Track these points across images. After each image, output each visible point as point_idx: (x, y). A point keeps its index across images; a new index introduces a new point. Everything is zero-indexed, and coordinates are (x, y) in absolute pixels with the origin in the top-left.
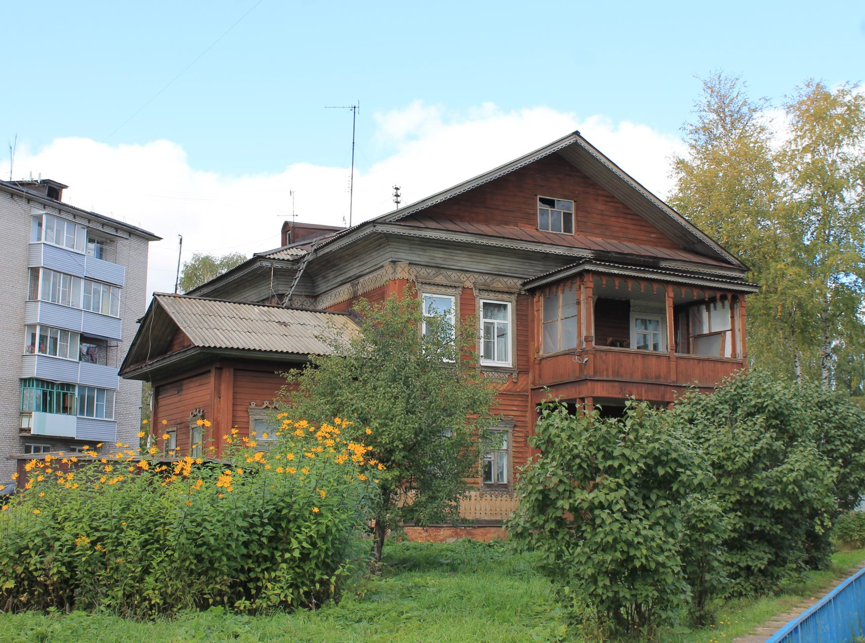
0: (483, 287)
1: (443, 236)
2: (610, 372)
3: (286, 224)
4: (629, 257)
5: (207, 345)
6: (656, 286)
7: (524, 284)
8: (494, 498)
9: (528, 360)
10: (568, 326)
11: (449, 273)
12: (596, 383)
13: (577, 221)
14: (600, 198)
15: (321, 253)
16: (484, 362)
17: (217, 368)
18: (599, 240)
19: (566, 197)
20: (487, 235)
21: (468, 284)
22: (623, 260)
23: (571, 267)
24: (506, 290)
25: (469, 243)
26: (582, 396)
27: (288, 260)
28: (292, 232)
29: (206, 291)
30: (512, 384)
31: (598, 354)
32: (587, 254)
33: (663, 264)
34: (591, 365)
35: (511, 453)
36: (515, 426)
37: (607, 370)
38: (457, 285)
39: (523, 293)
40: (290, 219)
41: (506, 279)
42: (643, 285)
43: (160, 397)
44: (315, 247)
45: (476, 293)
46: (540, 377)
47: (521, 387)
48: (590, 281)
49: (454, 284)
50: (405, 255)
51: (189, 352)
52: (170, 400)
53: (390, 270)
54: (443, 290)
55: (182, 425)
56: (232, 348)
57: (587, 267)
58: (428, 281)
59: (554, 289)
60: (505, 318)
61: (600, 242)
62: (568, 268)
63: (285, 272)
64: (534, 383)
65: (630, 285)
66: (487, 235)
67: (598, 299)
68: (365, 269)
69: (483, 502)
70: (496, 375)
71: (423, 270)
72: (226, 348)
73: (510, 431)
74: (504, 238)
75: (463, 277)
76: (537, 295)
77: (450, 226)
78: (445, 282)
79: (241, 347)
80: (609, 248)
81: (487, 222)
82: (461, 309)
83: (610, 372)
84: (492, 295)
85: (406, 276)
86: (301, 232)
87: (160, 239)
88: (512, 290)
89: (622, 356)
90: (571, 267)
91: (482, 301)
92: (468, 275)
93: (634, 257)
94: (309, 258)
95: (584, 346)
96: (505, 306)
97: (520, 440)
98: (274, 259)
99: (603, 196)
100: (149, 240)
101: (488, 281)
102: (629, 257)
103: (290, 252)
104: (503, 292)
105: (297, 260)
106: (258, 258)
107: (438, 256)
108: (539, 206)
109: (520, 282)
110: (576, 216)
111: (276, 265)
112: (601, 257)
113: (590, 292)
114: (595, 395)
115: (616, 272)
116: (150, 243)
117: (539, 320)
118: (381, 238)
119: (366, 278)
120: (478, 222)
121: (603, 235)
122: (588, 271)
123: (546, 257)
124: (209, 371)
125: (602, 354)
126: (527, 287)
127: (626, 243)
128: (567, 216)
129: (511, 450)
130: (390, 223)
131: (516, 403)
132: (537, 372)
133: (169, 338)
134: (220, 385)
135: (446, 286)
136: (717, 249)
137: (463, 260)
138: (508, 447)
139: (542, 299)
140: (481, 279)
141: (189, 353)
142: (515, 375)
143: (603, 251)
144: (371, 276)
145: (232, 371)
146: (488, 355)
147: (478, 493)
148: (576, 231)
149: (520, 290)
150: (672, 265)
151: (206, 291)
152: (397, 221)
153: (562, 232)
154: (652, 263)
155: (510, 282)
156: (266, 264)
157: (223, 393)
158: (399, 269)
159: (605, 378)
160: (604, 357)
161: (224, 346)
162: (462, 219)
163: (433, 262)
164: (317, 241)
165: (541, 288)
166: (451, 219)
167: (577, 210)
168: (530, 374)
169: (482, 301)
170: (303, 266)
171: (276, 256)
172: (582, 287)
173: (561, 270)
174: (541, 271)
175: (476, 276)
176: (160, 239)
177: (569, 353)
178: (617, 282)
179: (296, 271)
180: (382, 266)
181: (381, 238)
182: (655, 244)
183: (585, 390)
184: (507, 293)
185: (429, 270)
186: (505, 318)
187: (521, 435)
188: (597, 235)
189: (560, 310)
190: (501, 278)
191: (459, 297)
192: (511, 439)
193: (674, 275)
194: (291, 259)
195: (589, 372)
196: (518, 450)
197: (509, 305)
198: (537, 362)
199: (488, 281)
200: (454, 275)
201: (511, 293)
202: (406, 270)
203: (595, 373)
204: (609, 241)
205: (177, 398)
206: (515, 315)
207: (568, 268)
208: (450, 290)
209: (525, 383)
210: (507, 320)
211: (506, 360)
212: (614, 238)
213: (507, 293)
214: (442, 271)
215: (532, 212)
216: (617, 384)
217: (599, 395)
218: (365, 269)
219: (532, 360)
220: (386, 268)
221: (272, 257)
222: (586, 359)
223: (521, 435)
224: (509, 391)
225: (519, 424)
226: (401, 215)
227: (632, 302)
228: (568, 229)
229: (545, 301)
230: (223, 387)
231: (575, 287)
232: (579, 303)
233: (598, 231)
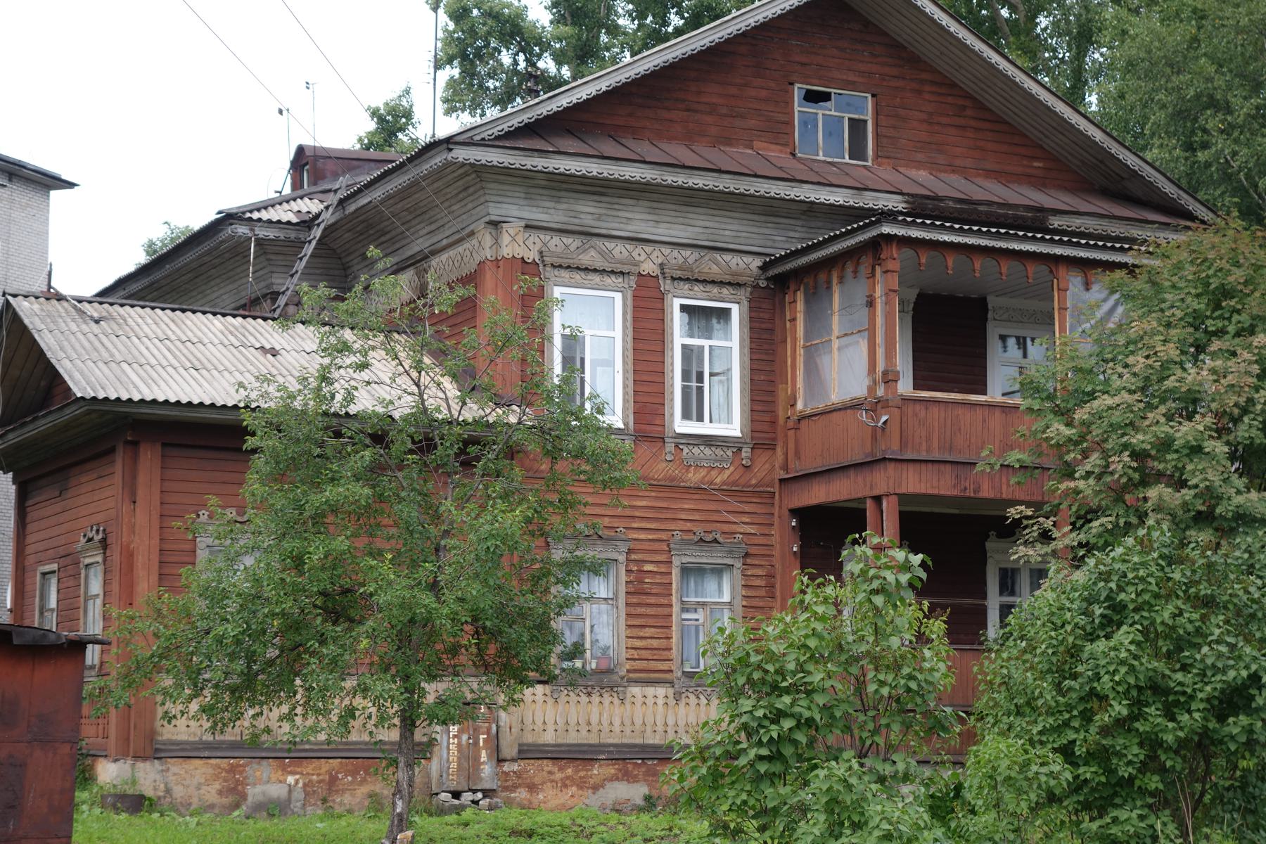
0: (678, 274)
1: (594, 168)
2: (935, 444)
3: (301, 150)
4: (981, 208)
5: (101, 395)
6: (1033, 269)
7: (764, 267)
8: (704, 701)
9: (774, 423)
10: (853, 357)
11: (610, 245)
12: (904, 466)
13: (877, 136)
14: (927, 88)
15: (352, 208)
16: (682, 426)
17: (127, 442)
18: (922, 175)
19: (852, 86)
20: (684, 167)
21: (649, 267)
22: (967, 214)
23: (854, 231)
24: (728, 278)
25: (648, 184)
26: (876, 492)
27: (289, 223)
28: (307, 165)
29: (134, 287)
30: (741, 470)
31: (910, 408)
32: (894, 203)
33: (1055, 222)
34: (894, 430)
35: (740, 610)
36: (747, 555)
37: (929, 439)
38: (626, 269)
39: (763, 284)
40: (308, 141)
41: (727, 257)
42: (1006, 266)
43: (30, 502)
44: (340, 195)
45: (666, 285)
46: (797, 454)
47: (760, 475)
48: (896, 259)
49: (619, 268)
50: (514, 210)
51: (67, 411)
52: (45, 510)
53: (488, 240)
54: (596, 278)
55: (68, 560)
56: (154, 401)
57: (887, 229)
58: (565, 262)
59: (822, 277)
60: (727, 336)
61: (924, 180)
62: (848, 233)
63: (281, 246)
64: (785, 467)
65: (977, 266)
66: (684, 167)
67: (921, 296)
68: (441, 238)
69: (682, 709)
70: (707, 451)
71: (556, 240)
72: (142, 401)
73: (738, 564)
74: (719, 171)
75: (639, 252)
76: (792, 287)
77: (609, 148)
78: (600, 264)
79: (173, 400)
80: (942, 190)
81: (689, 138)
82: (635, 319)
83: (935, 444)
84: (698, 288)
85: (520, 252)
86: (330, 166)
87: (71, 185)
88: (741, 280)
89: (960, 411)
90: (854, 231)
91: (677, 303)
92: (648, 249)
93: (993, 209)
94: (328, 218)
95: (880, 392)
96: (724, 314)
97: (758, 582)
98: (260, 220)
99: (933, 83)
100: (49, 187)
101: (691, 261)
102: (981, 208)
103: (295, 206)
104: (721, 284)
105: (308, 223)
106: (229, 218)
107: (587, 212)
108: (799, 107)
109: (758, 262)
110: (877, 125)
111: (262, 232)
112: (924, 208)
113: (894, 281)
114: (904, 490)
115: (946, 238)
116: (53, 193)
117: (795, 340)
118: (466, 174)
119: (444, 257)
120: (670, 139)
121: (933, 167)
122: (889, 238)
123: (811, 210)
124: (112, 451)
125: (918, 407)
126: (772, 273)
127: (980, 181)
128: (857, 127)
129: (739, 602)
130: (483, 143)
131: (747, 508)
132: (791, 445)
133: (43, 383)
134: (134, 477)
135: (603, 272)
136: (1169, 189)
137: (637, 220)
138: (733, 598)
139: (800, 296)
140: (677, 257)
141: (70, 413)
142: (746, 452)
143: (927, 197)
144: (451, 253)
145: (159, 448)
146: (693, 409)
147: (671, 691)
148: (877, 156)
149: (757, 278)
150: (1076, 223)
151: (134, 287)
152: (498, 138)
153: (847, 160)
154: (1034, 222)
155: (735, 261)
156: (242, 230)
157: (141, 493)
158: (506, 239)
159: (923, 456)
160: (923, 413)
161: (136, 398)
162: (636, 133)
163: (574, 224)
164: (343, 183)
165: (798, 274)
166: (614, 133)
167: (877, 113)
168: (779, 450)
169: (677, 303)
170: (317, 233)
171: (264, 215)
172: (878, 269)
173: (835, 238)
174: (802, 239)
175: (666, 250)
176: (71, 185)
177: (854, 406)
178: (951, 260)
179: (301, 244)
180: (472, 234)
181: (466, 174)
182: (1040, 183)
183: (881, 481)
184: (730, 284)
185: (568, 240)
186: (727, 336)
187: (759, 572)
188: (919, 165)
189: (836, 318)
190: (717, 256)
191: (630, 294)
192: (740, 581)
193: (1069, 243)
194: (295, 220)
195: (891, 446)
196: (639, 643)
197: (735, 309)
198: (791, 424)
199: (691, 261)
200: (620, 250)
201: (738, 285)
202: (520, 239)
203: (904, 444)
204: (942, 175)
205: (57, 508)
206: (746, 330)
207: (848, 233)
208: (609, 280)
209: (767, 468)
210: (729, 346)
211: (729, 421)
212: (954, 169)
213: (730, 284)
214: (599, 242)
215: (782, 118)
216: (948, 467)
217: (911, 490)
218: (441, 238)
219: (781, 421)
220: (479, 236)
221: (256, 215)
222: (884, 418)
223: (759, 572)
224: (735, 483)
225: (753, 550)
226: (505, 127)
227: (992, 301)
228: (857, 151)
229: (807, 302)
230: (142, 478)
231: (864, 269)
232: (871, 304)
233: (920, 157)
